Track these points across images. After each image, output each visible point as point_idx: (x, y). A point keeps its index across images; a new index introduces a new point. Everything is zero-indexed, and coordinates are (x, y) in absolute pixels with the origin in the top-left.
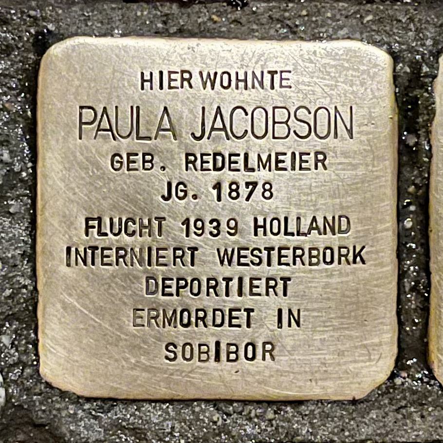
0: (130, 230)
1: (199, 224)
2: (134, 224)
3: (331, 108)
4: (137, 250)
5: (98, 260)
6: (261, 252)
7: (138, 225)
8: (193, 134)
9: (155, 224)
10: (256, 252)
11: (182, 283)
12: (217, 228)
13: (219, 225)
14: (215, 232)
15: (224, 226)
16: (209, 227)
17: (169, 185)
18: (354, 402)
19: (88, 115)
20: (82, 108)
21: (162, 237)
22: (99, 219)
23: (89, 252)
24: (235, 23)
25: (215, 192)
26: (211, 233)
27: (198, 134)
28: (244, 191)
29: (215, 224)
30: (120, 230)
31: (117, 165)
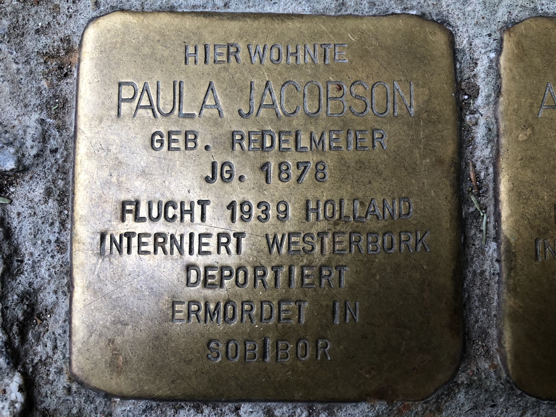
0: (170, 215)
1: (246, 208)
2: (174, 208)
3: (160, 254)
4: (178, 238)
5: (134, 250)
6: (313, 238)
7: (179, 209)
8: (239, 111)
9: (197, 209)
10: (308, 239)
11: (227, 273)
12: (265, 212)
13: (267, 209)
14: (263, 216)
15: (272, 212)
16: (255, 211)
17: (214, 165)
18: (122, 10)
19: (127, 93)
20: (120, 84)
21: (233, 200)
22: (137, 203)
23: (125, 240)
24: (232, 308)
25: (229, 212)
26: (259, 218)
27: (245, 112)
28: (294, 173)
29: (264, 208)
30: (159, 216)
31: (157, 145)
